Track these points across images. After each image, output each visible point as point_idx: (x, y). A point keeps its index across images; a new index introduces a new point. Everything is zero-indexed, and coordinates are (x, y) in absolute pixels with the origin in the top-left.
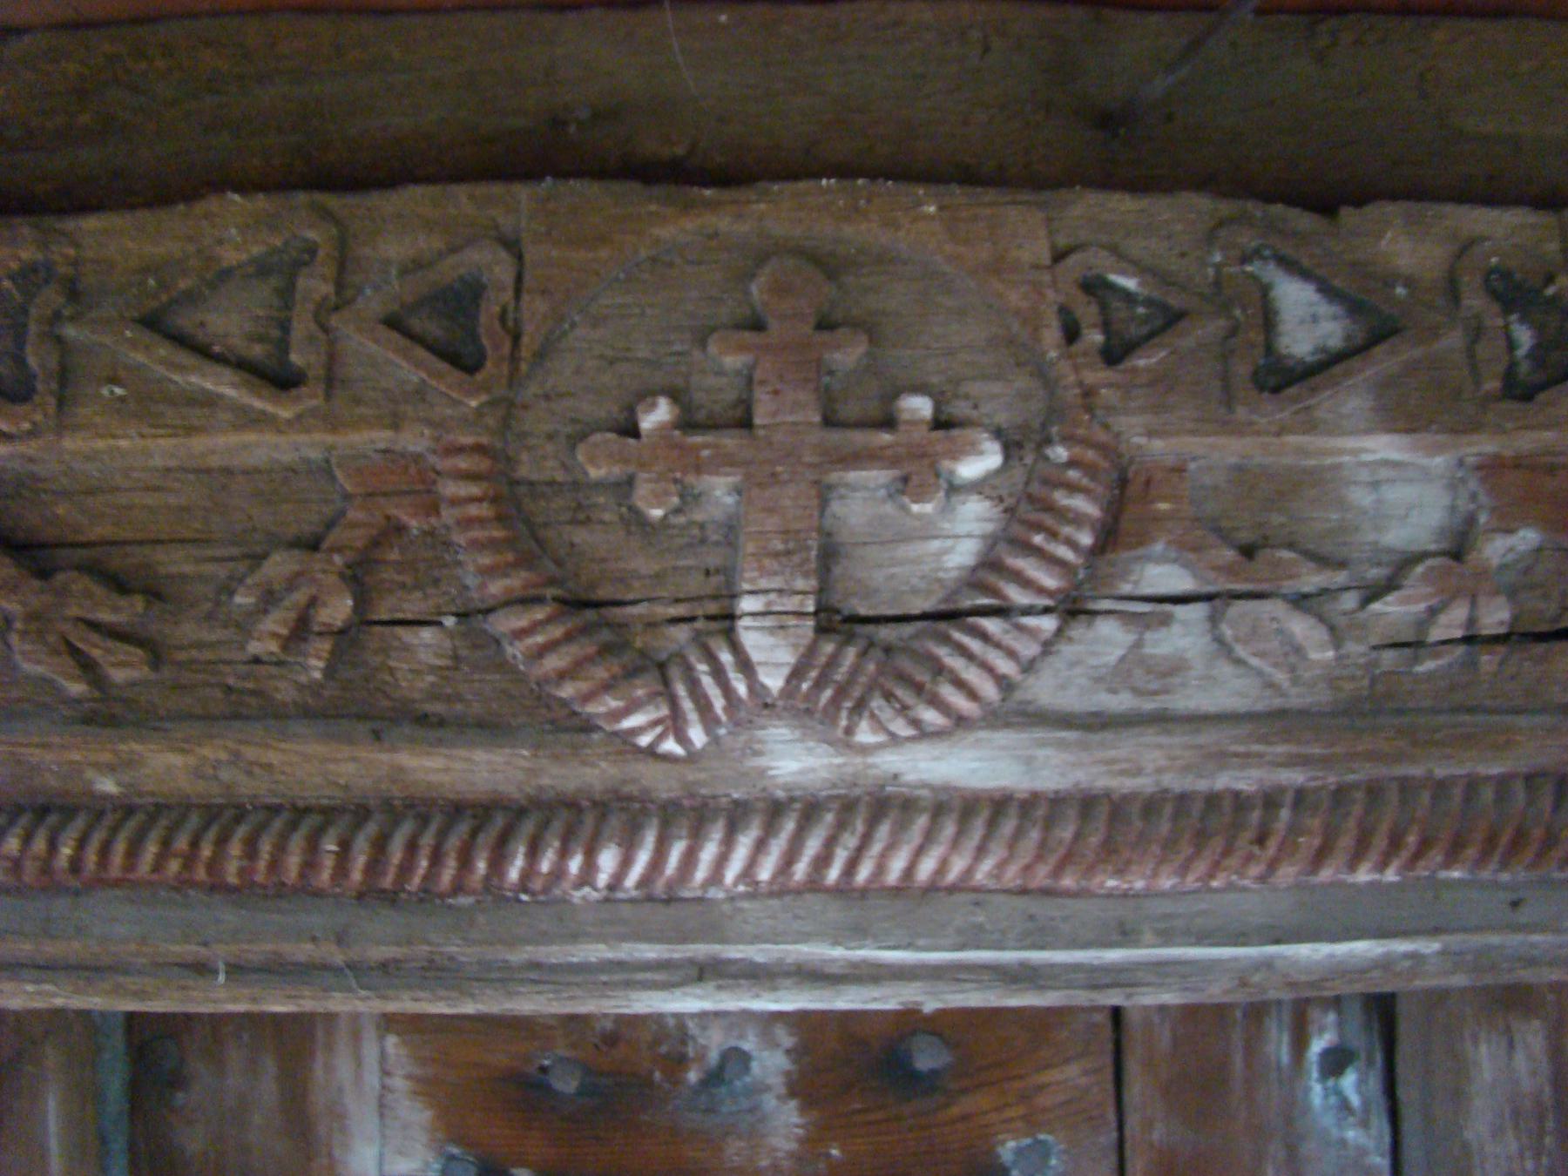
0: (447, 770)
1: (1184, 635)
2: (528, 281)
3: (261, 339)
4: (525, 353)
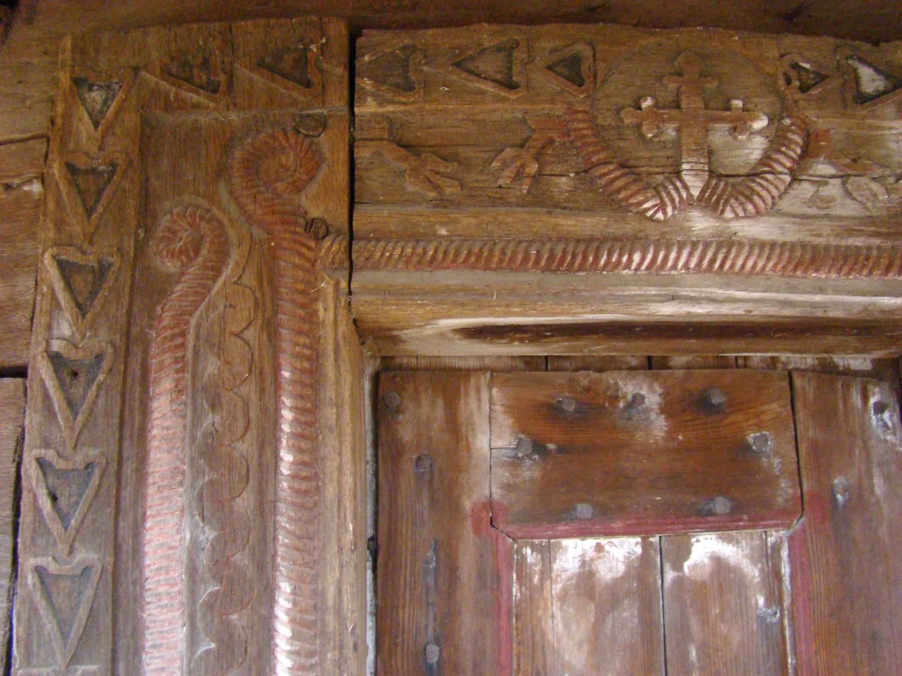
0: (575, 225)
1: (833, 189)
2: (598, 56)
3: (500, 72)
4: (598, 81)
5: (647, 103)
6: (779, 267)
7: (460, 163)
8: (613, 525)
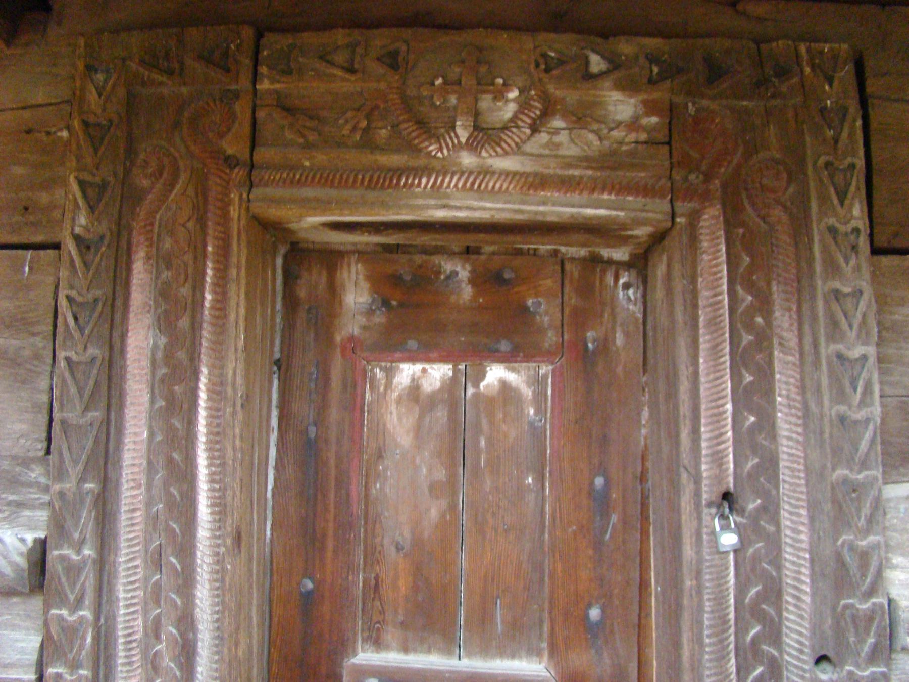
1: (563, 137)
5: (439, 82)
6: (518, 188)
7: (318, 119)
8: (431, 355)
